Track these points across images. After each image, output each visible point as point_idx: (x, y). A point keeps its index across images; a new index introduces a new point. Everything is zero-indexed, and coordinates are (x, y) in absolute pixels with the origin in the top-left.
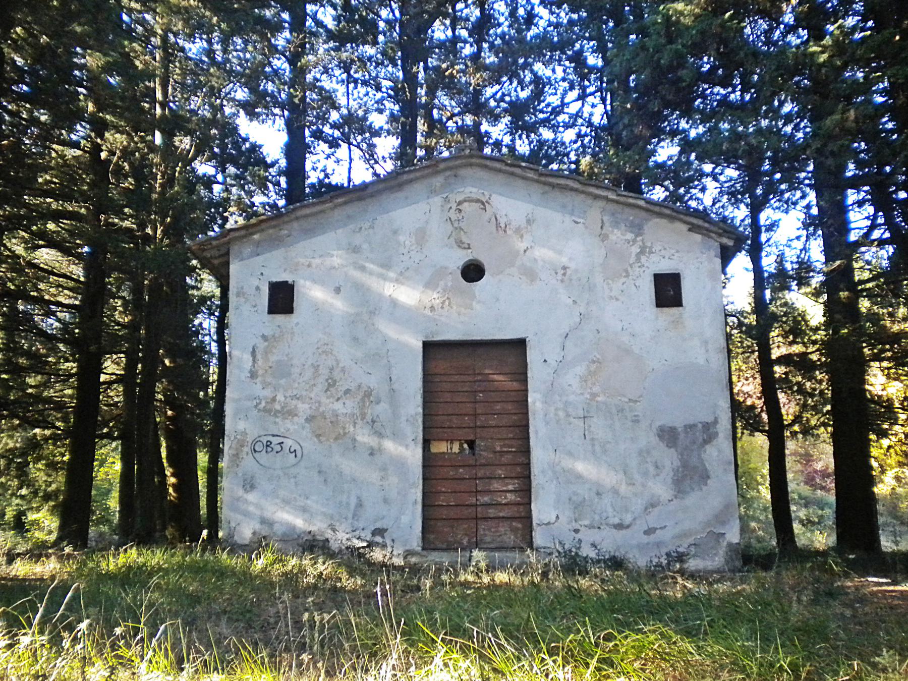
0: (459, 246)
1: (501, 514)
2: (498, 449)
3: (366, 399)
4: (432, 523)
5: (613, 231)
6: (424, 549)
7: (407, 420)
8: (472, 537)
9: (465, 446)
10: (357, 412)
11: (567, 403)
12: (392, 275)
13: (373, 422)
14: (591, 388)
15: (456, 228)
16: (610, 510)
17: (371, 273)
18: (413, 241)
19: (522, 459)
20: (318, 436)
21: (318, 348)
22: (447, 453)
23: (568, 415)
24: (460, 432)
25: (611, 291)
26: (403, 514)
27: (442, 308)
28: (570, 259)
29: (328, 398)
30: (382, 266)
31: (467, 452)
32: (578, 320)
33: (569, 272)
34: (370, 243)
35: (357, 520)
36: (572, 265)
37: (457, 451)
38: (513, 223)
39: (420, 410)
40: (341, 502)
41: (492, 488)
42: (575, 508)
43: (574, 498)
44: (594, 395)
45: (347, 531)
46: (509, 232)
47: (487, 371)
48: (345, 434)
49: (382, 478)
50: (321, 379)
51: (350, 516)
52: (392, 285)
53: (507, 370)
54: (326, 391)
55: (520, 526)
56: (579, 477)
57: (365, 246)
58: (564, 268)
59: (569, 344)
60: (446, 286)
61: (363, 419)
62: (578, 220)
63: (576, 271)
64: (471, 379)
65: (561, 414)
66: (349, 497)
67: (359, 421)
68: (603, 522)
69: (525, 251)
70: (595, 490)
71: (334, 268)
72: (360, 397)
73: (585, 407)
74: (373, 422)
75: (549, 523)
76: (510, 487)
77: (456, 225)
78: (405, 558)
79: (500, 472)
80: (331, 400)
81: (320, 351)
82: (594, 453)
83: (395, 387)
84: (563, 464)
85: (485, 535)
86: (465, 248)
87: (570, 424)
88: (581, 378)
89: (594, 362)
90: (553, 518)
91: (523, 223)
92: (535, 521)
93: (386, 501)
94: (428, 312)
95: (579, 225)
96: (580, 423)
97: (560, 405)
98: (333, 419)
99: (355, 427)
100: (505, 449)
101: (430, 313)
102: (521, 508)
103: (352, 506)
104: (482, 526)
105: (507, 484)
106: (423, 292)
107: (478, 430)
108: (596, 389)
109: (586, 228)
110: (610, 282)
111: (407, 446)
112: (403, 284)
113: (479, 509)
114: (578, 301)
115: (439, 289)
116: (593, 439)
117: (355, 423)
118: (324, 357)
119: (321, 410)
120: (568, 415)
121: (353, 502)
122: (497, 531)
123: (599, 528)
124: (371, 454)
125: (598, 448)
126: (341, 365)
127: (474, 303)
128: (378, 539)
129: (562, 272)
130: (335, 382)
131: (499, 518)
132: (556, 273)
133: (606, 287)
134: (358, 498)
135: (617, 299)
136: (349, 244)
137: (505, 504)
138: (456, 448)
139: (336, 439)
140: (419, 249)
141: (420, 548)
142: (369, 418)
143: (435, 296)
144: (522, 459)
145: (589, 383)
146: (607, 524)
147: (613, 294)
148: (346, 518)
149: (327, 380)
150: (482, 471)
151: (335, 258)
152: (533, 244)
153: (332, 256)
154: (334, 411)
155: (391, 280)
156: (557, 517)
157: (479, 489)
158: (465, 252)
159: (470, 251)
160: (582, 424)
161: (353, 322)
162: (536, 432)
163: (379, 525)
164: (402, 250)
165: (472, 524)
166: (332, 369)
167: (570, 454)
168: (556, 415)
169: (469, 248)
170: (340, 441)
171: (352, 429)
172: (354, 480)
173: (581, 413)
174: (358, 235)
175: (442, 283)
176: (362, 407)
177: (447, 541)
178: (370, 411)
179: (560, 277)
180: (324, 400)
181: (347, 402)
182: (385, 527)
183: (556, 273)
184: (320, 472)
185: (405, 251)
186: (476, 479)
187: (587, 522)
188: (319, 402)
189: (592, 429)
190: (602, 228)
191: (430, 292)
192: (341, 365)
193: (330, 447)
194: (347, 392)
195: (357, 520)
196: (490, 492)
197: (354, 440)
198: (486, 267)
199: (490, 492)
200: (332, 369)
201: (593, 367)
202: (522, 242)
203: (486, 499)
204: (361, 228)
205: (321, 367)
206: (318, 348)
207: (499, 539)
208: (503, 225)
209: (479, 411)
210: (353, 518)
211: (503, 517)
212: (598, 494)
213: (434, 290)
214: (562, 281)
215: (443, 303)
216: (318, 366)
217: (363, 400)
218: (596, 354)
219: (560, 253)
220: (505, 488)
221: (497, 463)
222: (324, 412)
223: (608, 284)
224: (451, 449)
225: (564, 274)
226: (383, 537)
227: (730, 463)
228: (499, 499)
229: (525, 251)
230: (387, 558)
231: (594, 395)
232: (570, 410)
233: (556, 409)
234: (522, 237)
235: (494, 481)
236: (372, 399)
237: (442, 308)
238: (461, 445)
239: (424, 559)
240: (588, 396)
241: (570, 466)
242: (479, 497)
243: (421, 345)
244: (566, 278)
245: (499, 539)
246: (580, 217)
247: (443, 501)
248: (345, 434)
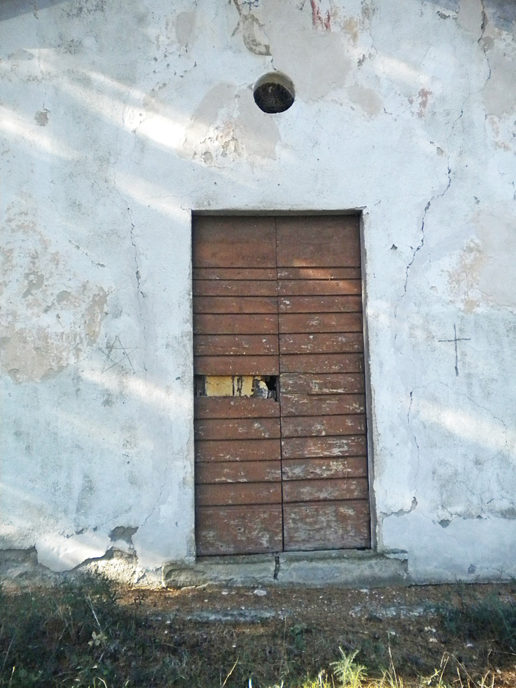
0: (251, 49)
1: (322, 496)
2: (316, 390)
3: (97, 309)
4: (210, 511)
5: (500, 34)
6: (199, 557)
7: (167, 346)
8: (276, 534)
9: (263, 385)
10: (81, 331)
11: (428, 318)
12: (137, 94)
13: (110, 348)
14: (466, 293)
15: (246, 18)
16: (495, 487)
17: (100, 91)
18: (173, 35)
19: (355, 407)
20: (13, 372)
21: (10, 220)
22: (232, 398)
23: (430, 337)
24: (254, 362)
25: (497, 133)
26: (163, 503)
27: (224, 155)
28: (434, 78)
29: (29, 306)
30: (121, 78)
31: (265, 395)
32: (445, 181)
33: (431, 100)
34: (97, 37)
35: (86, 514)
36: (437, 89)
37: (250, 393)
38: (341, 13)
39: (189, 328)
40: (55, 484)
41: (306, 453)
42: (443, 486)
43: (441, 470)
44: (471, 304)
45: (67, 532)
46: (334, 28)
47: (297, 264)
48: (61, 368)
49: (126, 443)
50: (17, 274)
51: (73, 507)
52: (137, 112)
53: (329, 260)
54: (25, 295)
55: (351, 512)
56: (449, 436)
57: (89, 42)
58: (424, 93)
59: (430, 220)
60: (231, 117)
61: (91, 342)
62: (447, 13)
63: (442, 99)
64: (270, 274)
65: (420, 335)
66: (69, 476)
67: (84, 347)
68: (485, 508)
69: (360, 62)
70: (472, 456)
71: (35, 79)
72: (84, 306)
73: (458, 323)
74: (110, 348)
75: (401, 512)
76: (336, 451)
77: (245, 11)
78: (168, 575)
79: (319, 427)
80: (36, 310)
81: (13, 224)
82: (471, 398)
83: (144, 288)
84: (424, 415)
85: (297, 530)
86: (261, 54)
87: (433, 350)
88: (450, 276)
89: (470, 250)
90: (408, 504)
91: (357, 14)
92: (380, 508)
93: (133, 481)
94: (199, 161)
95: (448, 21)
96: (450, 349)
97: (418, 321)
98: (40, 343)
99: (77, 356)
100: (326, 391)
101: (203, 164)
102: (354, 484)
103: (76, 493)
104: (292, 514)
105: (331, 446)
106: (192, 126)
107: (284, 360)
108: (474, 294)
109: (459, 26)
110: (496, 119)
111: (168, 389)
112: (156, 111)
113: (287, 487)
114: (446, 150)
115: (219, 123)
116: (469, 375)
117: (78, 350)
118: (20, 235)
119: (18, 326)
120: (430, 337)
121: (78, 482)
122: (316, 523)
123: (479, 517)
124: (107, 402)
125: (477, 391)
126: (52, 250)
127: (278, 148)
128: (122, 544)
129: (420, 100)
130: (41, 278)
131: (319, 501)
132: (411, 102)
133: (489, 128)
134: (86, 476)
135: (506, 148)
136: (61, 38)
137: (327, 479)
138: (247, 390)
139: (45, 377)
140: (183, 52)
141: (193, 559)
142: (102, 341)
143: (213, 133)
144: (355, 407)
145: (463, 284)
146: (491, 511)
147: (500, 139)
148: (66, 511)
149: (27, 276)
150: (291, 427)
151: (35, 62)
152: (373, 51)
153: (31, 57)
154: (40, 329)
155: (135, 104)
156: (415, 501)
157: (286, 455)
158: (260, 59)
159: (269, 58)
160: (452, 351)
161: (71, 175)
162: (381, 365)
163: (122, 522)
164: (153, 52)
165: (276, 511)
166: (35, 257)
167: (434, 399)
168: (411, 335)
169: (268, 54)
170: (53, 381)
171: (72, 361)
172: (78, 446)
173: (451, 334)
174: (76, 21)
175: (223, 112)
176: (90, 324)
177: (235, 541)
178: (103, 331)
179: (416, 107)
180: (22, 310)
181: (63, 314)
182: (133, 525)
183: (411, 102)
184: (18, 434)
185: (159, 55)
186: (280, 439)
187: (460, 509)
188: (14, 314)
189: (468, 359)
190: (483, 27)
191: (203, 127)
192: (52, 250)
193: (35, 391)
194: (63, 296)
195: (86, 514)
196: (303, 459)
197: (78, 379)
198: (297, 87)
199: (303, 459)
200: (35, 257)
201: (470, 258)
202: (354, 46)
203: (298, 471)
204: (81, 9)
205: (15, 254)
206: (10, 220)
207: (317, 537)
208: (324, 17)
209: (284, 329)
210: (78, 510)
211: (325, 500)
212: (477, 462)
213: (210, 124)
214: (420, 115)
215: (226, 146)
216: (11, 251)
217: (90, 310)
218: (474, 236)
219: (416, 66)
220: (326, 453)
221: (315, 412)
222: (22, 331)
223: (493, 123)
224: (239, 390)
225: (424, 104)
226: (130, 541)
227: (293, 293)
228: (318, 471)
229: (360, 62)
230: (136, 577)
231: (471, 304)
232: (433, 327)
233: (412, 327)
234: (355, 36)
235: (310, 442)
236: (106, 309)
237: (224, 155)
238: (256, 384)
239: (200, 577)
240: (462, 306)
241: (434, 419)
242: (286, 469)
243: (189, 218)
244: (426, 111)
245: (317, 537)
246: (447, 7)
247: (227, 475)
248: (61, 368)
